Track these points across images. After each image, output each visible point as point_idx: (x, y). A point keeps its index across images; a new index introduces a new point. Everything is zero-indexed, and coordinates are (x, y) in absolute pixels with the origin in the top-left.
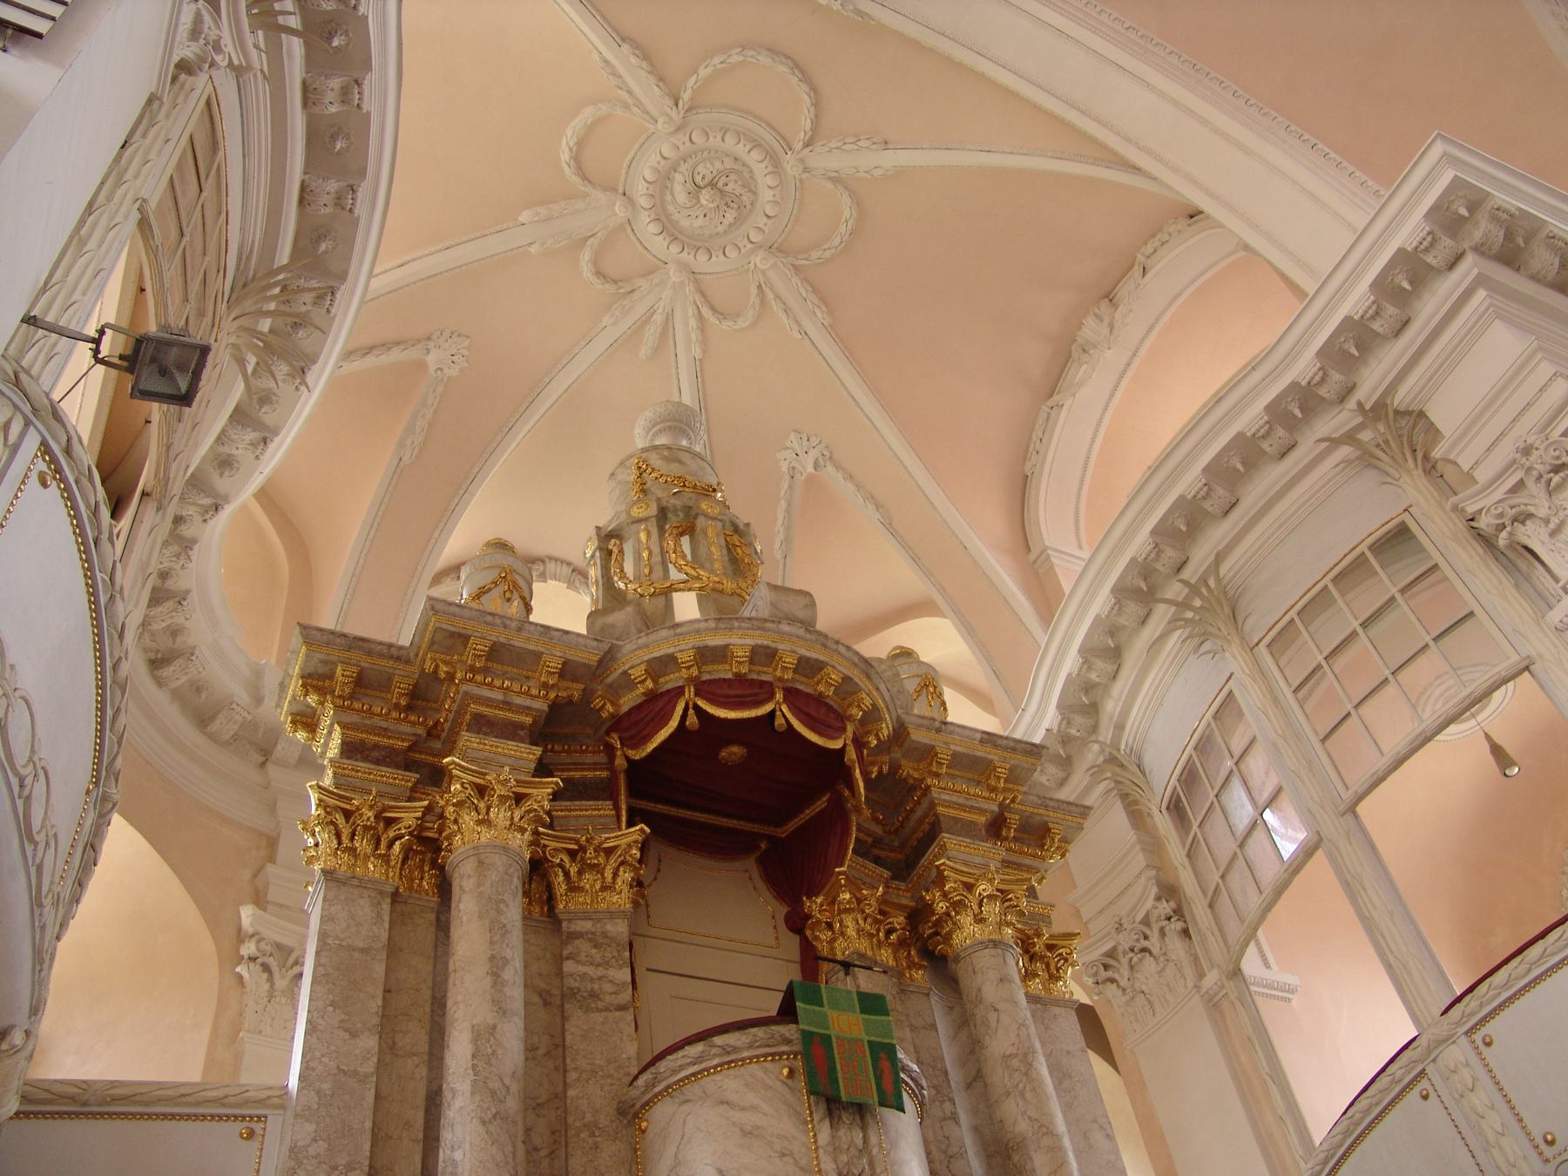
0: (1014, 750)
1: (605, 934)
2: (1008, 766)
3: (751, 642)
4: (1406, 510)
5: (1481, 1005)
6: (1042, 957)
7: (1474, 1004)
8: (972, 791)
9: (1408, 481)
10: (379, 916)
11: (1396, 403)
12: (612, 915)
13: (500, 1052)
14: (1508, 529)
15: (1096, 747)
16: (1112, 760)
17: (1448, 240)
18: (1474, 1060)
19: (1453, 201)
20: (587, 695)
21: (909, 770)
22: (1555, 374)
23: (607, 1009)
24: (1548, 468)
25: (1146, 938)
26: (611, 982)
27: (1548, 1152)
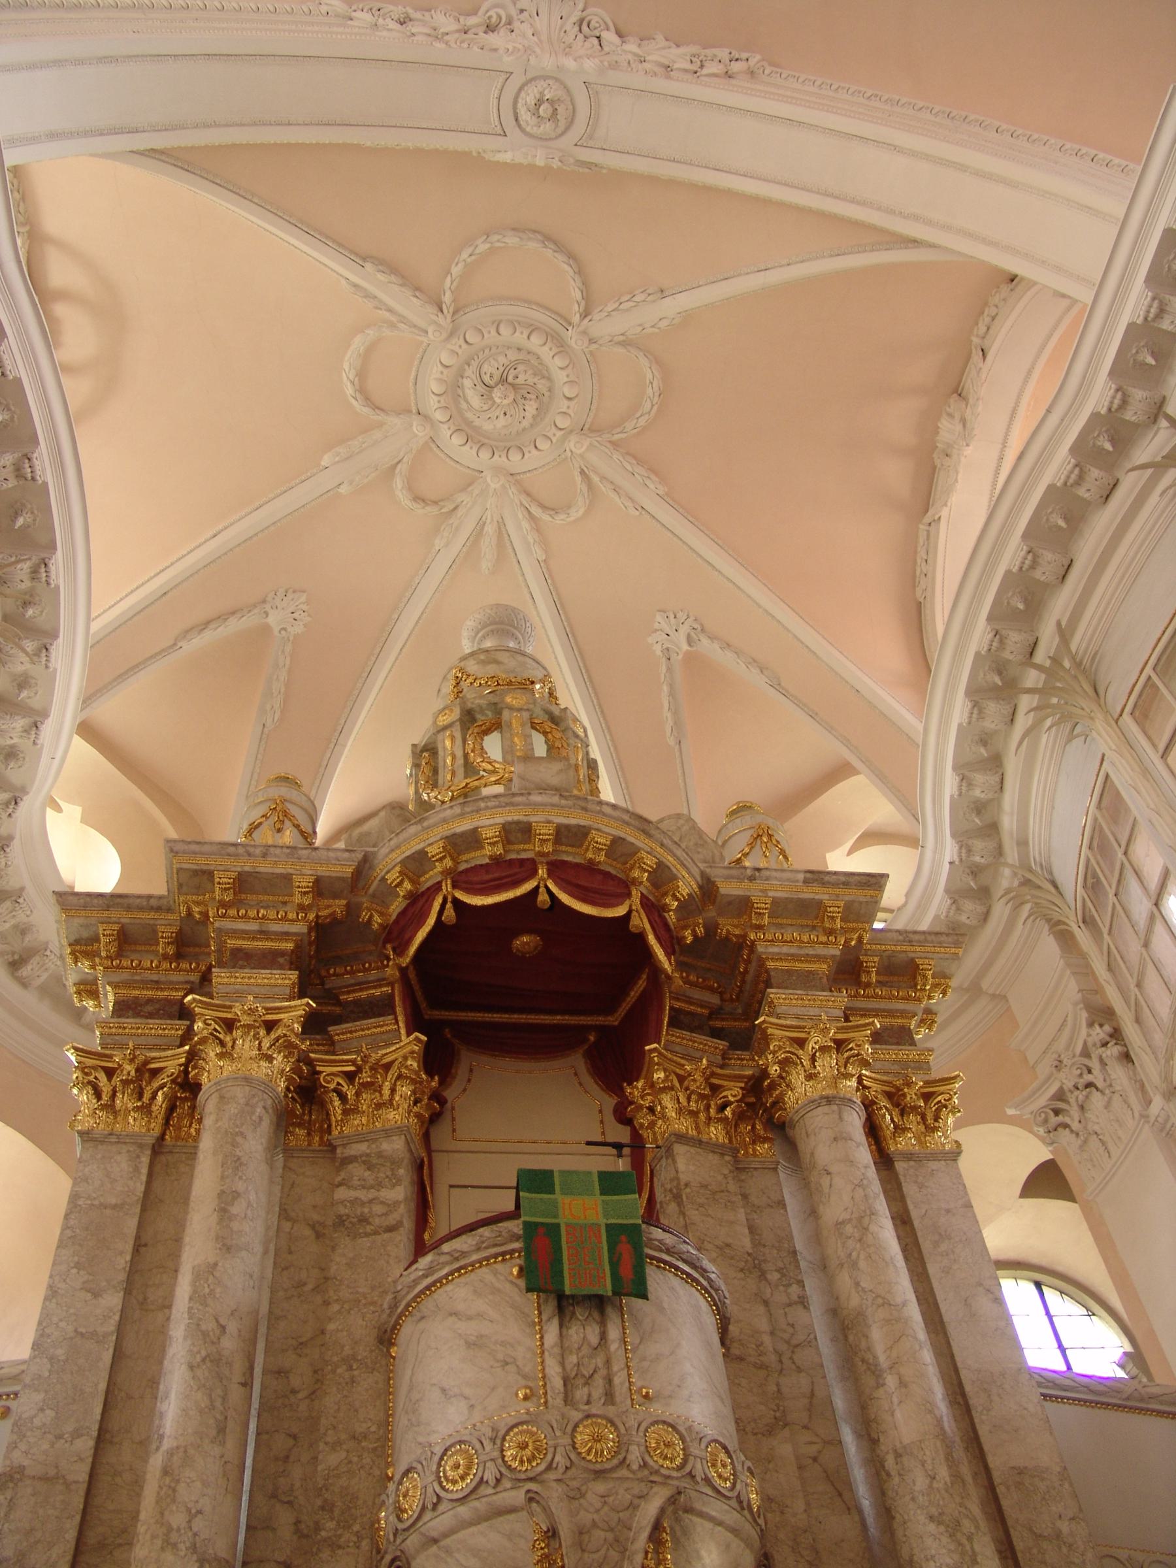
1: (380, 1155)
3: (500, 820)
8: (805, 938)
10: (137, 1169)
12: (388, 1133)
13: (218, 1290)
20: (352, 910)
21: (728, 927)
23: (376, 1233)
26: (382, 1203)
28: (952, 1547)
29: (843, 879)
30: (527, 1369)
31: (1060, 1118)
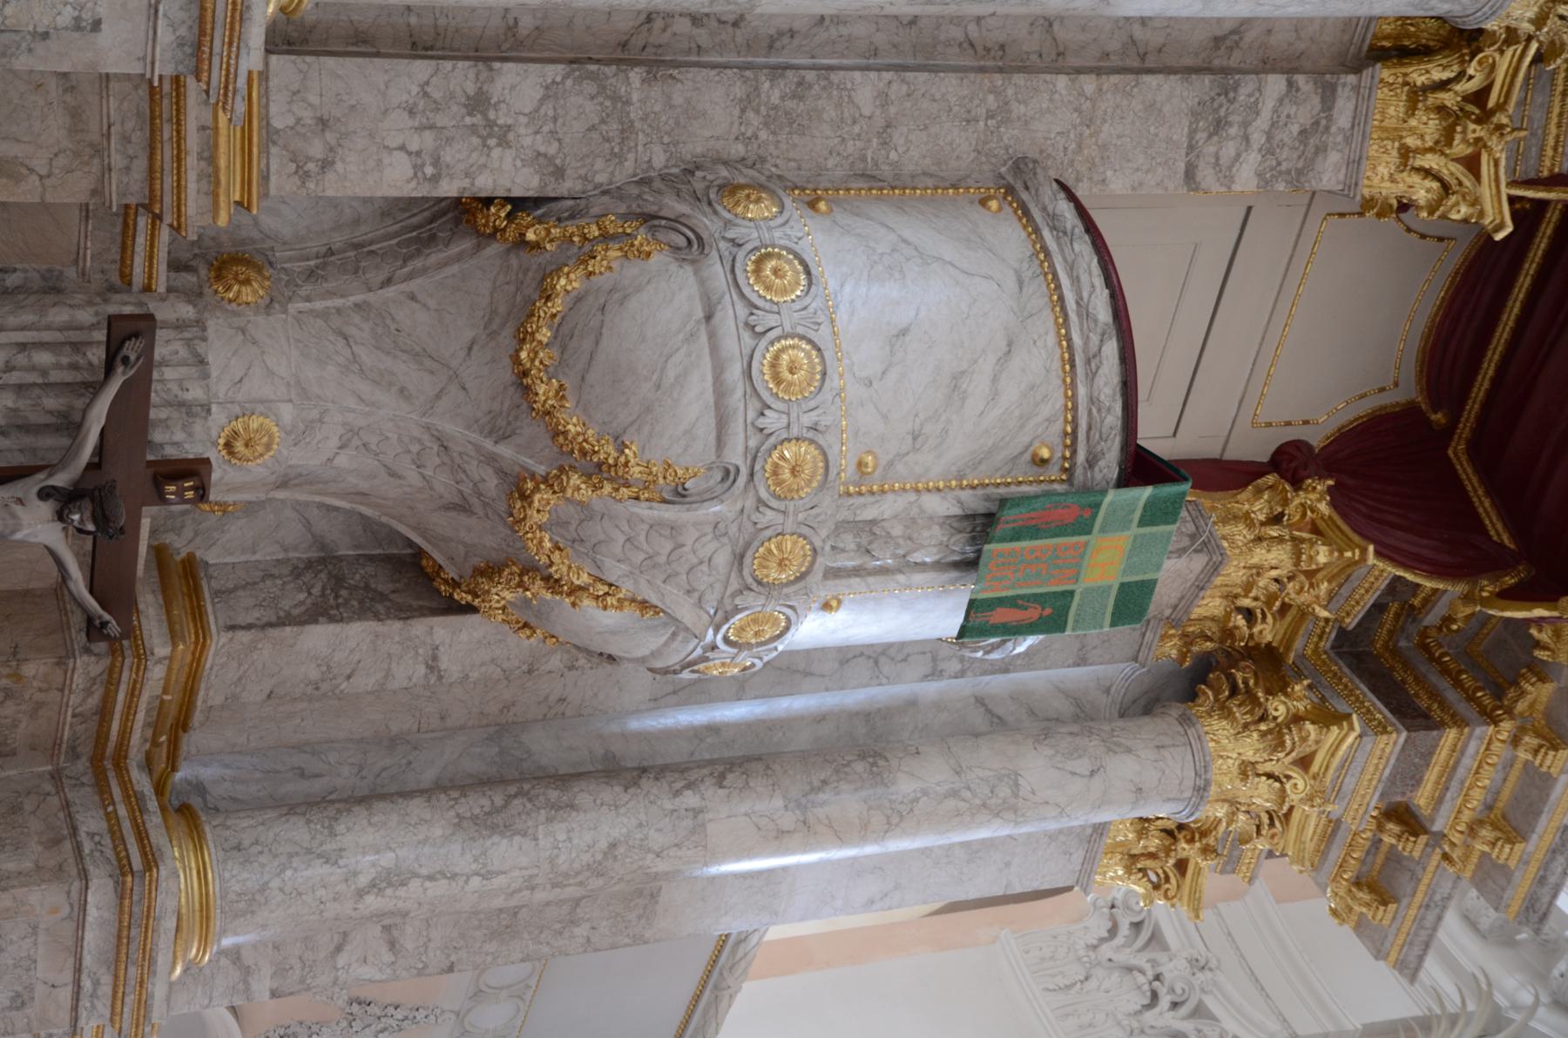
1: (1321, 150)
6: (1168, 851)
15: (1526, 998)
25: (1175, 1005)
28: (576, 865)
30: (900, 467)
31: (1124, 930)
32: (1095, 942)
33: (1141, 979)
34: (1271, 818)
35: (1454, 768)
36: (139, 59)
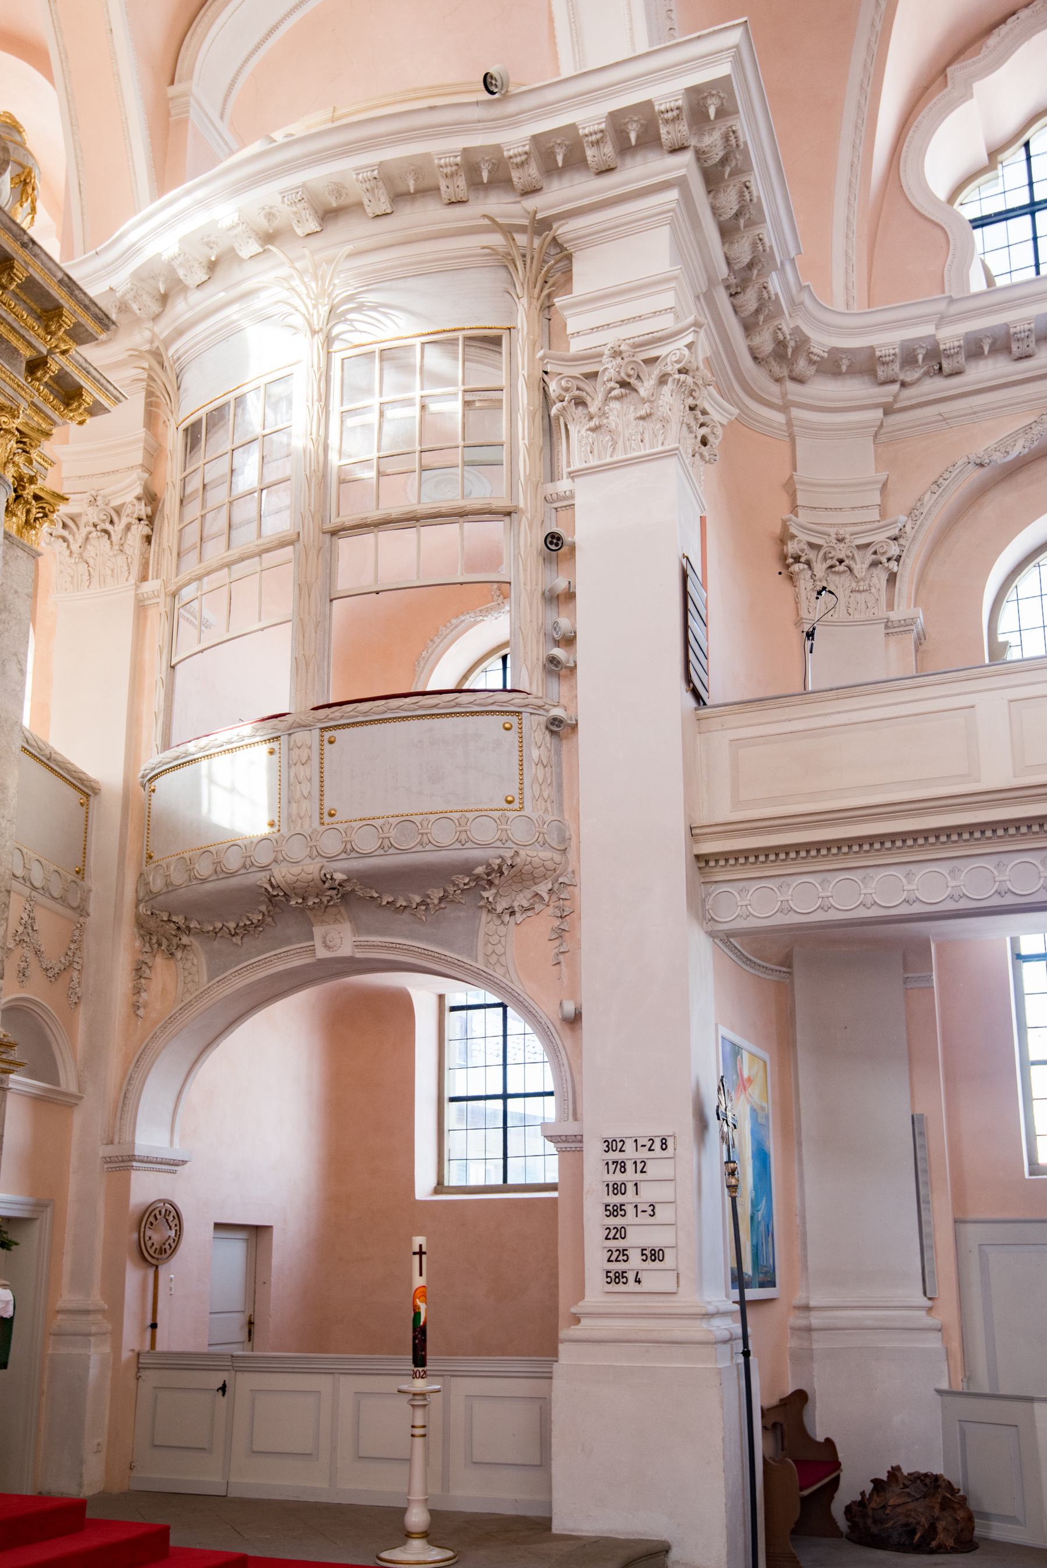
0: (86, 308)
2: (73, 321)
4: (509, 329)
5: (342, 717)
6: (27, 502)
7: (338, 714)
9: (526, 305)
11: (559, 232)
14: (565, 403)
15: (147, 334)
16: (157, 355)
17: (686, 127)
18: (316, 747)
19: (713, 95)
22: (671, 308)
24: (619, 379)
25: (112, 522)
27: (327, 819)
29: (87, 302)
31: (65, 533)
32: (69, 551)
33: (94, 534)
34: (21, 442)
35: (12, 328)
36: (573, 481)
